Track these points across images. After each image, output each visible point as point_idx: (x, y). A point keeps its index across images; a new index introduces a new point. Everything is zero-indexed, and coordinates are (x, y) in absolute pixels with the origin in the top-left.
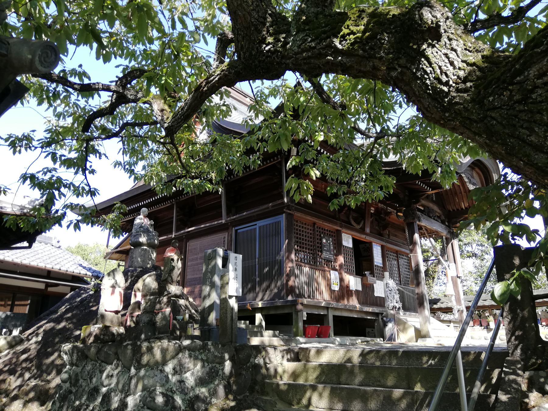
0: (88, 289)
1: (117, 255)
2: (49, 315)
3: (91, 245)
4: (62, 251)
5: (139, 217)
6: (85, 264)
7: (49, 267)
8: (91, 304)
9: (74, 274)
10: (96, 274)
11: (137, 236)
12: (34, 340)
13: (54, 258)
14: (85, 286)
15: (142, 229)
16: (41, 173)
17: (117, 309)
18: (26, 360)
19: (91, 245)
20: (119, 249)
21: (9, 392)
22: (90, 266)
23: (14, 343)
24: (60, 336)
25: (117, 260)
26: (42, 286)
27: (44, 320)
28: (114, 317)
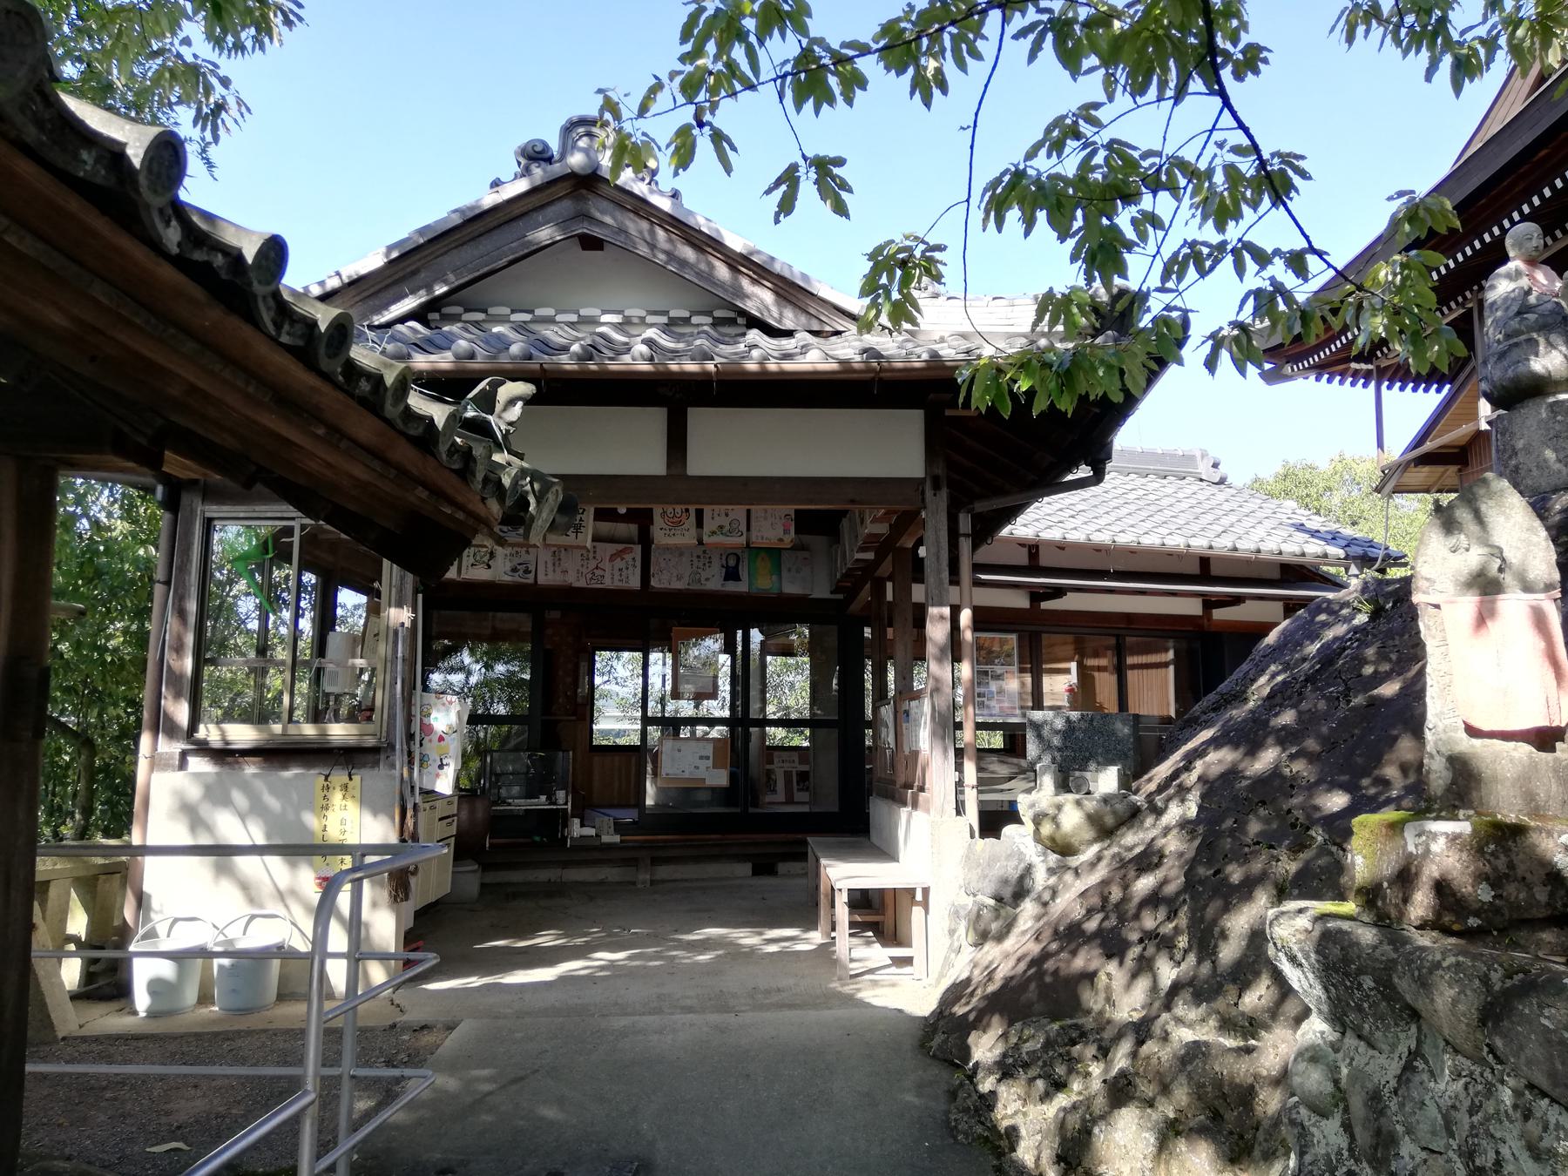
0: (1346, 604)
1: (1423, 474)
2: (1217, 708)
3: (1324, 465)
4: (1233, 491)
5: (1502, 270)
6: (1315, 523)
7: (1199, 544)
8: (1368, 670)
9: (1285, 558)
10: (1358, 551)
11: (1514, 355)
12: (1174, 813)
13: (1210, 517)
14: (1330, 595)
15: (1532, 317)
16: (1043, 152)
17: (1540, 721)
18: (1154, 899)
19: (1324, 465)
20: (1429, 446)
21: (1108, 1034)
22: (1334, 527)
23: (1109, 821)
24: (1262, 812)
25: (1427, 491)
26: (1193, 608)
27: (1207, 725)
28: (1534, 766)
